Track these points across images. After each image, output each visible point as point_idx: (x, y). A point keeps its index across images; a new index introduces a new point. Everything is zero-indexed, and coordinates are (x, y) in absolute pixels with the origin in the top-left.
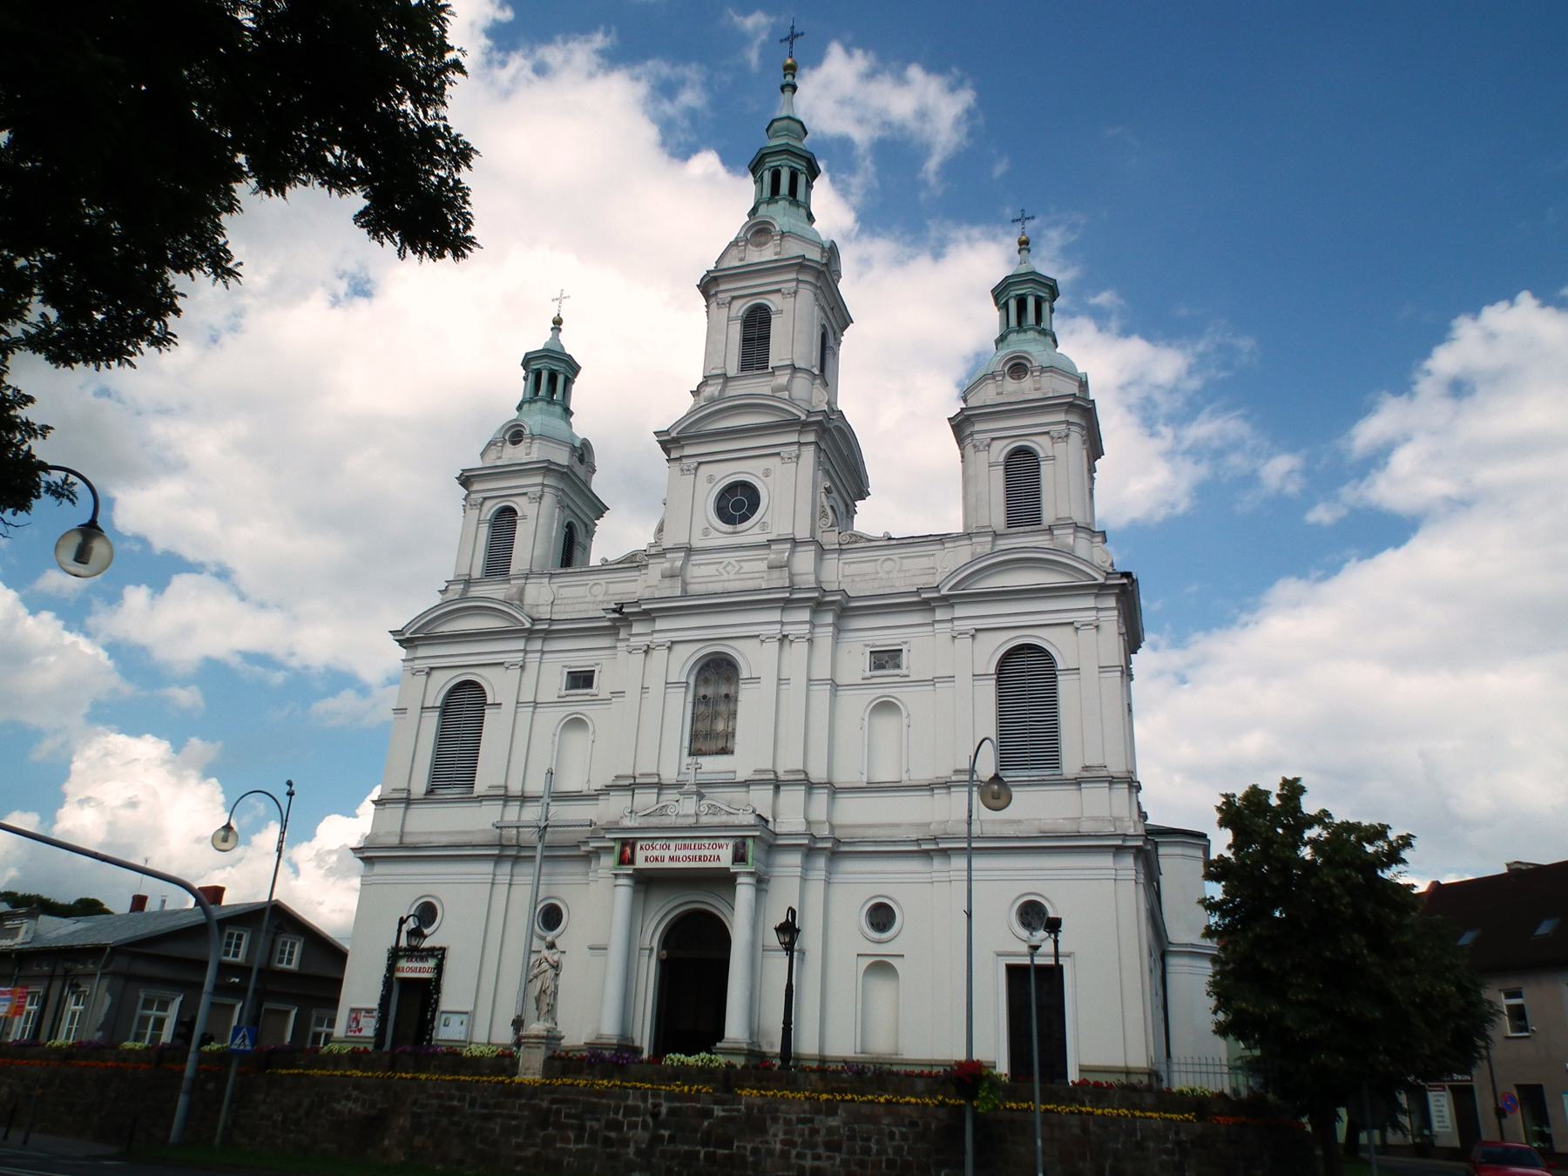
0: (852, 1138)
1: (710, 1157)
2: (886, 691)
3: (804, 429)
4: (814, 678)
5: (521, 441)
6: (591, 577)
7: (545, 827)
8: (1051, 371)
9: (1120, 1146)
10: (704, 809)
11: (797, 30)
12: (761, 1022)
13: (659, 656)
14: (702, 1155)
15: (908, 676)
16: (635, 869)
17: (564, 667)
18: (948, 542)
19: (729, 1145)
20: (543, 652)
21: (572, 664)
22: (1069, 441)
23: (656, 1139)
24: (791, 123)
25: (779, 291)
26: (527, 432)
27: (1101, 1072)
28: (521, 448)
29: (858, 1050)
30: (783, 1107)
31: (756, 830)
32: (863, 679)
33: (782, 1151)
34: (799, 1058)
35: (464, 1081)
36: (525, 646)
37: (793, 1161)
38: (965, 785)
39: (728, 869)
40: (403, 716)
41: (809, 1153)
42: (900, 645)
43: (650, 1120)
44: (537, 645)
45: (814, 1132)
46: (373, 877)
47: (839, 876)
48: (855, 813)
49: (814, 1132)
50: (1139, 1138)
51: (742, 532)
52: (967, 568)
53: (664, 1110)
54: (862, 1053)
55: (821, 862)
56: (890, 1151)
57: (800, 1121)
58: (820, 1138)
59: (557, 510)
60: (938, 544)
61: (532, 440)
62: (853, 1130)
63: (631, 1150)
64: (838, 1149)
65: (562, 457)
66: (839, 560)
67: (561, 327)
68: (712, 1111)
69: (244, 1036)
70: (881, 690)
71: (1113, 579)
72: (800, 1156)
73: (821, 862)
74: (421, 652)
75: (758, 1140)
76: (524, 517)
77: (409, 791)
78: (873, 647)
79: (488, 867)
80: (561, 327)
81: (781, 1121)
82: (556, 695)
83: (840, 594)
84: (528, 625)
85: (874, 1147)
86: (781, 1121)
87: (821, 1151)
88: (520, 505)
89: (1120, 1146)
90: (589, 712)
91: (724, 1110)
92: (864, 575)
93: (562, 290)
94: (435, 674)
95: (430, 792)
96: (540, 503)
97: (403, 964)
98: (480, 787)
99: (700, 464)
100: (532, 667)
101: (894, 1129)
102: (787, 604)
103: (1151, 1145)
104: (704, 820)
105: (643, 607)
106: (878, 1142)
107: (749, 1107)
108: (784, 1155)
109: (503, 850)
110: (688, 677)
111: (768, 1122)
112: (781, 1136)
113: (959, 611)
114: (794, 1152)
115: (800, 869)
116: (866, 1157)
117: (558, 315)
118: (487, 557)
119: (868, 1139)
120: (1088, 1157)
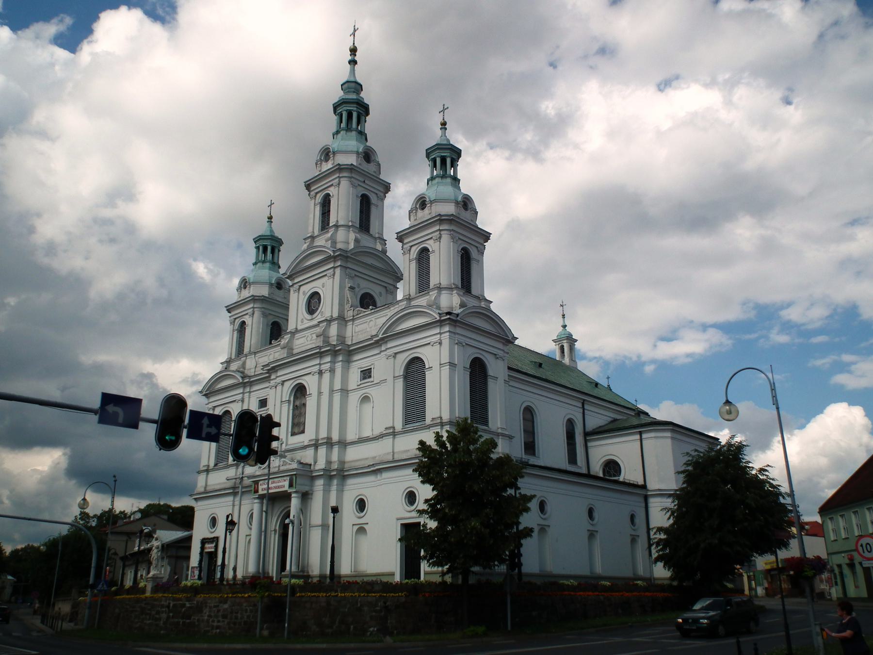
2: (364, 391)
3: (336, 259)
4: (335, 390)
5: (426, 207)
6: (368, 318)
7: (242, 478)
8: (436, 202)
10: (282, 463)
12: (310, 562)
13: (279, 388)
14: (181, 623)
15: (373, 382)
16: (259, 495)
17: (359, 368)
18: (431, 292)
19: (189, 619)
20: (250, 392)
21: (260, 396)
22: (441, 240)
23: (168, 617)
24: (350, 84)
25: (332, 185)
26: (428, 200)
27: (389, 575)
28: (426, 211)
29: (353, 571)
30: (209, 601)
31: (294, 471)
32: (358, 386)
33: (207, 619)
34: (340, 577)
35: (277, 596)
36: (440, 330)
38: (439, 425)
39: (287, 491)
40: (431, 371)
41: (216, 619)
42: (266, 396)
43: (167, 609)
45: (219, 611)
46: (382, 481)
47: (347, 487)
48: (354, 454)
49: (219, 611)
50: (359, 605)
51: (315, 318)
52: (389, 322)
53: (171, 605)
54: (354, 572)
56: (245, 617)
58: (220, 614)
59: (452, 243)
60: (387, 309)
61: (431, 204)
63: (162, 622)
65: (449, 209)
66: (353, 324)
67: (272, 220)
68: (185, 604)
69: (103, 584)
70: (361, 391)
71: (443, 316)
72: (213, 621)
74: (212, 399)
76: (433, 251)
77: (394, 428)
78: (361, 368)
79: (231, 498)
80: (272, 220)
81: (208, 607)
82: (356, 385)
83: (341, 346)
84: (438, 318)
85: (239, 615)
86: (208, 607)
87: (220, 619)
88: (431, 245)
89: (347, 610)
90: (372, 392)
91: (190, 604)
92: (362, 331)
94: (398, 356)
95: (216, 465)
96: (440, 242)
97: (207, 546)
99: (300, 286)
100: (246, 400)
101: (247, 608)
102: (321, 355)
104: (282, 468)
105: (271, 366)
108: (208, 621)
109: (235, 490)
110: (290, 397)
112: (207, 613)
113: (390, 345)
114: (211, 620)
115: (322, 486)
117: (443, 120)
120: (328, 616)
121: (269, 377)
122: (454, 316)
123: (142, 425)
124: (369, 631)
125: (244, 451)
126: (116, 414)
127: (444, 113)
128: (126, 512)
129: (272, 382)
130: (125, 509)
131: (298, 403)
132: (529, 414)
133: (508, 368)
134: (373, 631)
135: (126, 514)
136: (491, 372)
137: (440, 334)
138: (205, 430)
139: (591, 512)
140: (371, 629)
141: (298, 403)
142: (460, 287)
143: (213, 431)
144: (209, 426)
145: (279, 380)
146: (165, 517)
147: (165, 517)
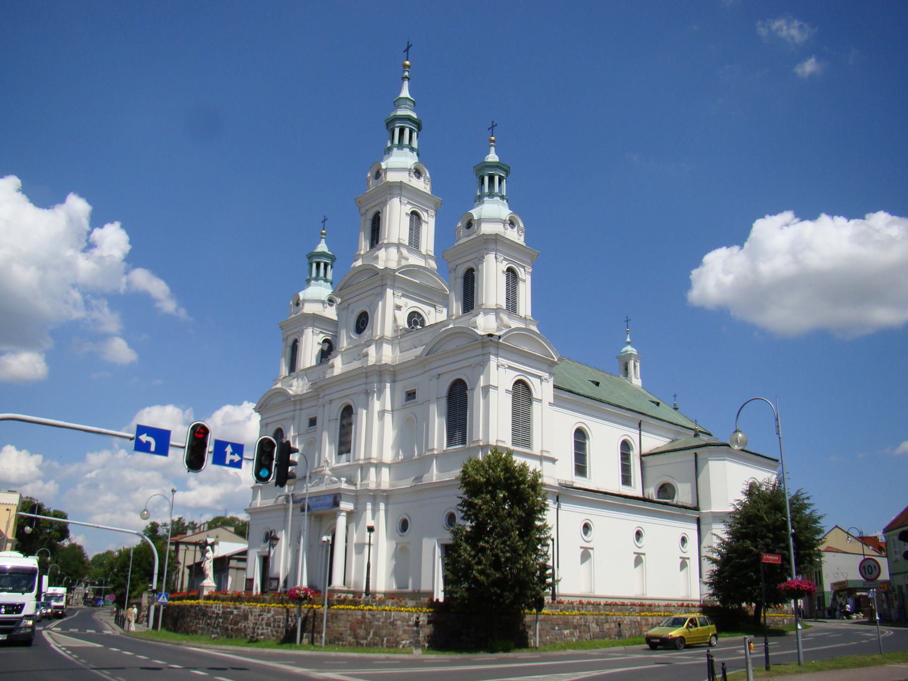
0: (274, 621)
9: (380, 623)
11: (410, 44)
19: (237, 625)
45: (263, 619)
55: (284, 507)
62: (275, 618)
72: (258, 628)
73: (284, 507)
75: (246, 622)
87: (264, 626)
93: (493, 122)
103: (399, 623)
107: (244, 611)
111: (250, 616)
114: (256, 627)
116: (279, 629)
118: (464, 287)
119: (279, 622)
121: (318, 395)
122: (496, 338)
123: (171, 451)
124: (401, 644)
125: (264, 473)
126: (148, 443)
127: (492, 130)
128: (195, 523)
129: (320, 400)
130: (556, 465)
131: (345, 422)
132: (580, 436)
133: (554, 387)
134: (406, 644)
135: (196, 524)
136: (535, 394)
137: (294, 410)
138: (229, 457)
139: (639, 534)
140: (404, 642)
141: (345, 422)
142: (505, 308)
143: (236, 458)
144: (232, 454)
145: (327, 398)
146: (232, 529)
147: (232, 529)
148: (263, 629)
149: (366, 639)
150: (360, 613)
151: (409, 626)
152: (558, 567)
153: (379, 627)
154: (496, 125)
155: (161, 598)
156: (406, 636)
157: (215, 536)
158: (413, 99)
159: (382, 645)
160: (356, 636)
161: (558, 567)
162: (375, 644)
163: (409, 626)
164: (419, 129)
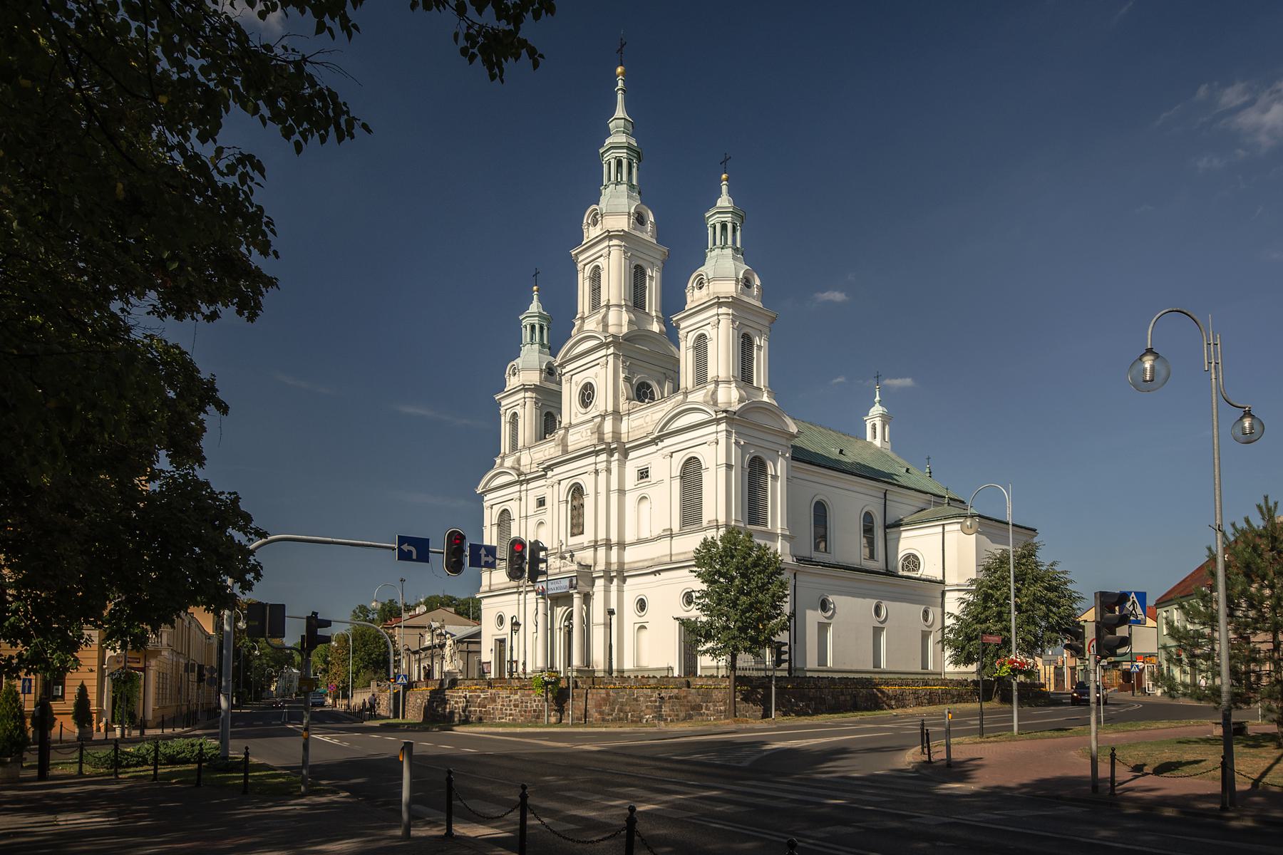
0: (522, 702)
1: (480, 711)
21: (639, 465)
37: (504, 711)
44: (524, 487)
53: (468, 696)
57: (506, 697)
58: (512, 703)
64: (518, 707)
69: (1134, 602)
72: (506, 710)
75: (494, 704)
76: (711, 339)
87: (512, 707)
98: (705, 523)
99: (572, 375)
103: (642, 699)
106: (530, 703)
108: (501, 709)
119: (527, 702)
121: (546, 474)
126: (410, 552)
138: (484, 559)
140: (647, 716)
141: (575, 503)
144: (485, 556)
146: (452, 610)
147: (452, 610)
148: (511, 710)
149: (612, 715)
150: (603, 691)
151: (651, 701)
152: (795, 643)
153: (622, 704)
154: (730, 158)
155: (400, 680)
156: (648, 711)
157: (441, 620)
158: (630, 120)
159: (627, 720)
160: (601, 713)
161: (795, 643)
162: (620, 719)
163: (651, 701)
164: (639, 160)
